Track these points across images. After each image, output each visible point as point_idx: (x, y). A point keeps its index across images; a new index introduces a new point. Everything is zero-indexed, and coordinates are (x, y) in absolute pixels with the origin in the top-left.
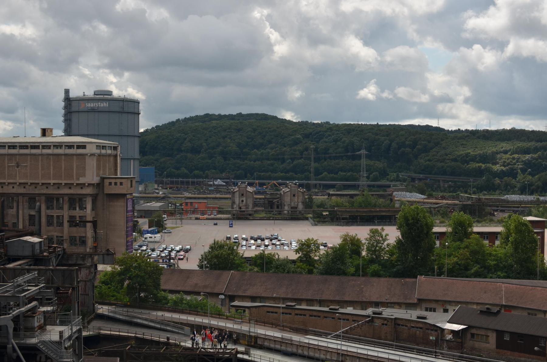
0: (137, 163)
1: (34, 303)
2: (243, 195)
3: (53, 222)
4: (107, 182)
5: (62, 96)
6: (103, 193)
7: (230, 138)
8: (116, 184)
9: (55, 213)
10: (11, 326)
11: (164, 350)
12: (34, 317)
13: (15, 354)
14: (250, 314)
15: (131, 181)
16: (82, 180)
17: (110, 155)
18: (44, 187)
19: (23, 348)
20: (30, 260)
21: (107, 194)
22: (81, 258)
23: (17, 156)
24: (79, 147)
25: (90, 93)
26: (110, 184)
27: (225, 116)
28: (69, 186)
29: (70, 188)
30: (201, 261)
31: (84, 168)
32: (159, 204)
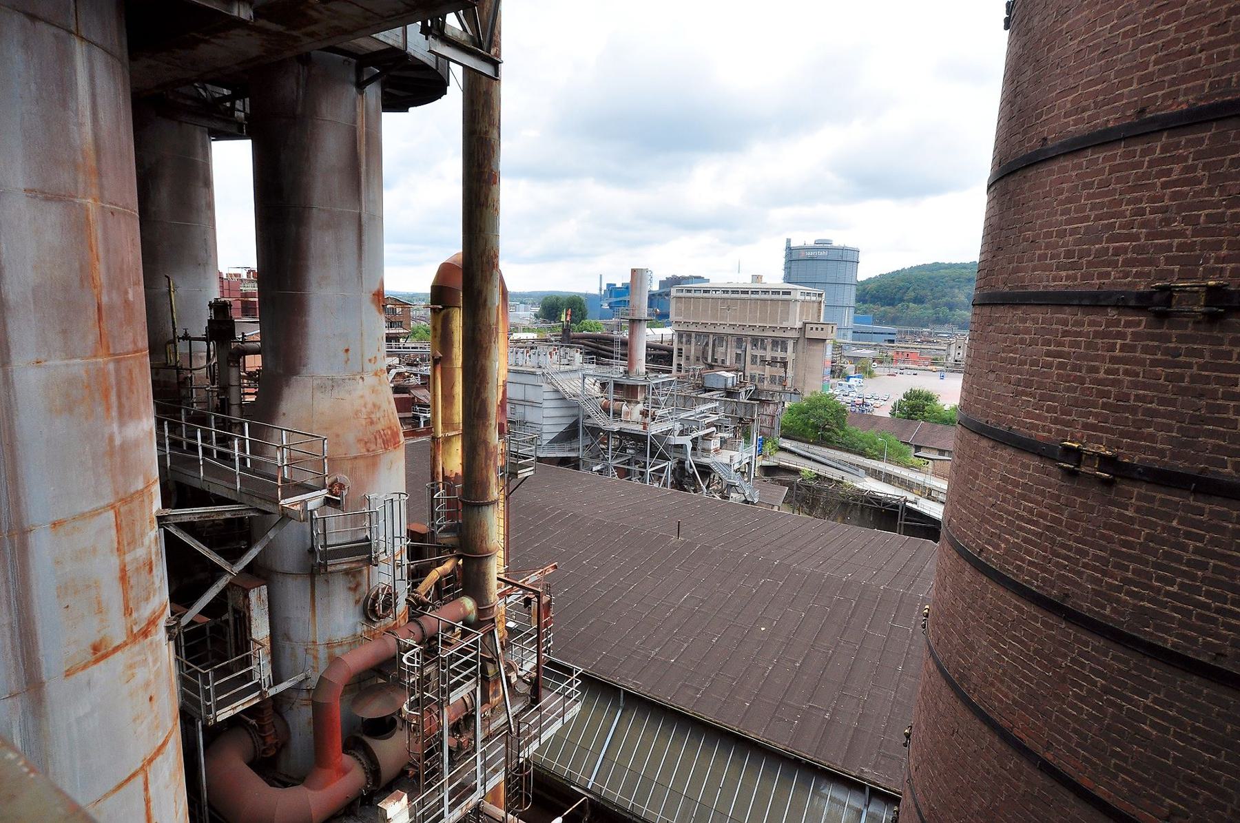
0: (852, 310)
2: (960, 347)
3: (756, 361)
5: (784, 246)
8: (817, 329)
10: (690, 446)
13: (692, 470)
17: (814, 302)
21: (809, 339)
24: (784, 293)
25: (811, 243)
27: (956, 264)
28: (774, 329)
29: (774, 331)
30: (894, 408)
31: (788, 313)
32: (868, 352)
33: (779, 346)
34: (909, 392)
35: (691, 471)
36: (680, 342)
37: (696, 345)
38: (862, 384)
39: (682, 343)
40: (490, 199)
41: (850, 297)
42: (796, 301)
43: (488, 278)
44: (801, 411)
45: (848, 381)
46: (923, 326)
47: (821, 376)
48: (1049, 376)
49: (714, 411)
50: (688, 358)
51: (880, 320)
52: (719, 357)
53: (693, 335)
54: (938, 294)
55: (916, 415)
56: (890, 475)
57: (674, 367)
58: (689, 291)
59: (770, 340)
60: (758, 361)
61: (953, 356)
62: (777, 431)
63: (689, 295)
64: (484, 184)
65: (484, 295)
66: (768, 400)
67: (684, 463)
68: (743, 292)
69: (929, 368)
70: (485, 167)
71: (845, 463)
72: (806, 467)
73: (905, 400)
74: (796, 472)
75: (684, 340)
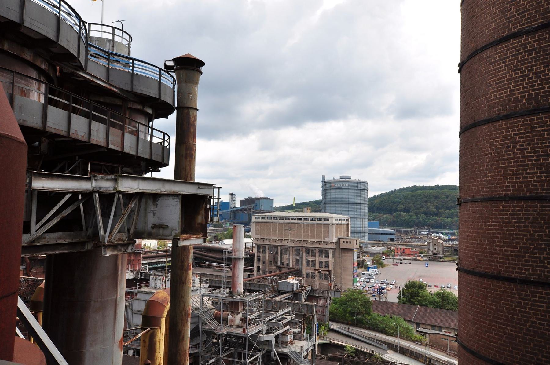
0: (366, 220)
1: (288, 327)
2: (435, 245)
3: (309, 264)
4: (341, 241)
5: (321, 179)
6: (339, 247)
7: (430, 202)
8: (347, 242)
9: (311, 258)
10: (274, 341)
11: (368, 361)
12: (287, 335)
13: (275, 358)
14: (430, 338)
15: (357, 241)
16: (326, 240)
17: (344, 224)
18: (305, 242)
19: (279, 354)
20: (291, 294)
22: (322, 292)
23: (290, 224)
24: (325, 220)
25: (337, 178)
26: (344, 242)
27: (427, 187)
28: (319, 243)
29: (320, 244)
31: (328, 232)
33: (324, 254)
34: (408, 283)
35: (275, 358)
36: (259, 251)
37: (269, 253)
38: (377, 273)
39: (260, 252)
40: (187, 279)
41: (364, 211)
42: (333, 225)
43: (185, 323)
44: (343, 303)
45: (368, 270)
46: (411, 227)
47: (351, 273)
48: (490, 316)
49: (288, 314)
50: (264, 262)
51: (383, 224)
52: (285, 261)
53: (267, 247)
54: (418, 206)
55: (414, 299)
56: (403, 348)
57: (255, 268)
58: (263, 218)
59: (317, 250)
60: (311, 264)
61: (432, 250)
62: (327, 316)
63: (264, 220)
64: (185, 272)
65: (182, 334)
66: (320, 296)
67: (270, 352)
68: (299, 219)
69: (418, 258)
70: (185, 262)
71: (373, 339)
72: (349, 344)
73: (406, 288)
74: (342, 347)
75: (261, 250)
